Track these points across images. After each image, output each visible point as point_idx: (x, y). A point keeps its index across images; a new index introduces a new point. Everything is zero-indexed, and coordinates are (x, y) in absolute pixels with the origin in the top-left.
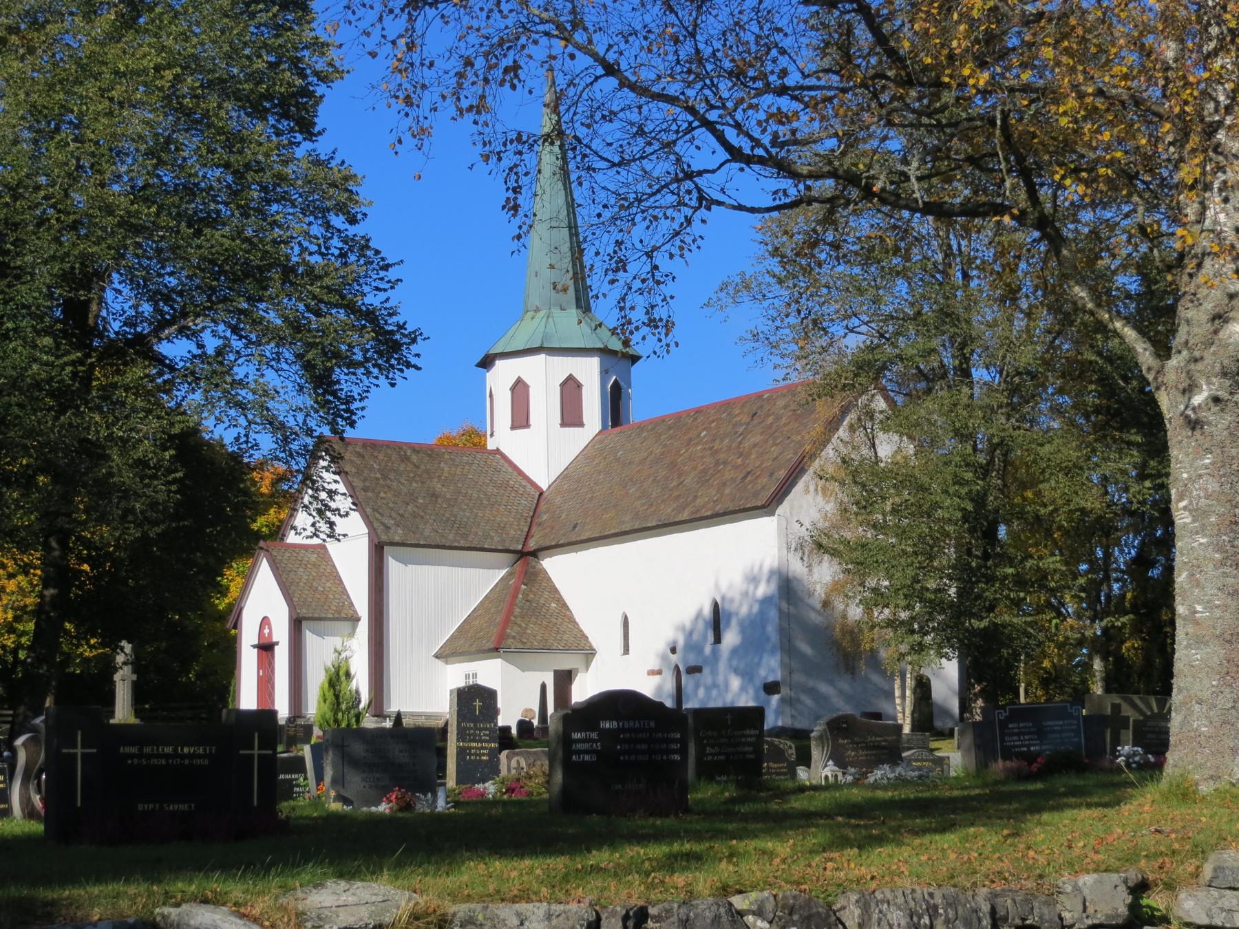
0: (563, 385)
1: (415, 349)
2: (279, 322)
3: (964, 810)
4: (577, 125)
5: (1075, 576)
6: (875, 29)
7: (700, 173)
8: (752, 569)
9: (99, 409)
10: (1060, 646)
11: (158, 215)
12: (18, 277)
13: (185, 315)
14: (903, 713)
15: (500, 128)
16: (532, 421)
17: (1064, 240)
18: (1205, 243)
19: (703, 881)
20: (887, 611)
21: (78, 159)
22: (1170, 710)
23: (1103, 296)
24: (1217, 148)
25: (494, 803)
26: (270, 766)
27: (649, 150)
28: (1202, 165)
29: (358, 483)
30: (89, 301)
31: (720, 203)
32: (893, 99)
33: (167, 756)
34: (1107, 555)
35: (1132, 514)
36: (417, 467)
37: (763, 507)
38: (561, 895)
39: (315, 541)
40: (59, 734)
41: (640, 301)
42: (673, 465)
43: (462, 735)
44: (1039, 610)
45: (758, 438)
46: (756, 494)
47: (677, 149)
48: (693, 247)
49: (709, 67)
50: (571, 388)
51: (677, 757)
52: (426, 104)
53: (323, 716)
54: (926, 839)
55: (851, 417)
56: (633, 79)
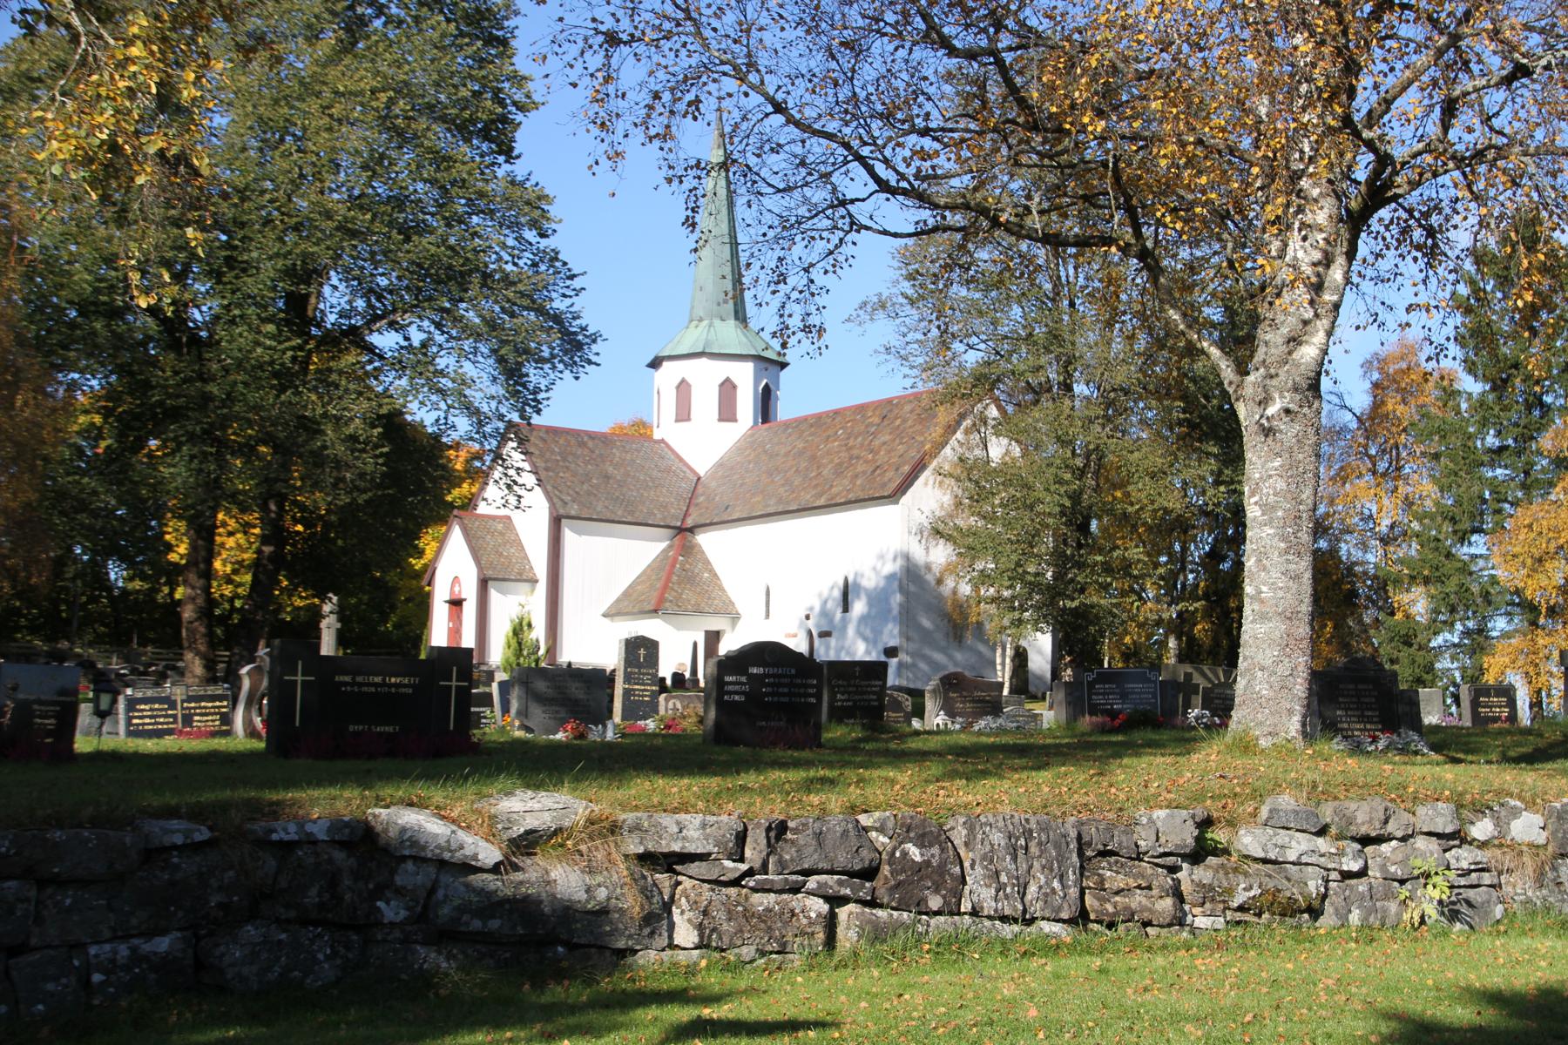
0: (722, 385)
1: (594, 348)
2: (477, 320)
3: (1056, 754)
4: (749, 154)
5: (1156, 565)
6: (1009, 82)
7: (852, 201)
9: (315, 389)
10: (1141, 625)
11: (373, 220)
12: (244, 270)
13: (394, 311)
14: (1003, 673)
15: (682, 156)
17: (1162, 270)
18: (1286, 275)
19: (835, 802)
20: (992, 590)
21: (301, 168)
22: (1235, 680)
23: (1193, 320)
24: (1299, 193)
25: (654, 735)
26: (465, 699)
27: (809, 179)
28: (1288, 205)
29: (541, 464)
30: (308, 296)
31: (867, 228)
32: (1020, 142)
33: (376, 685)
34: (1184, 549)
35: (1207, 514)
37: (889, 497)
38: (714, 809)
39: (503, 512)
40: (282, 663)
41: (797, 310)
42: (813, 458)
43: (628, 678)
44: (1124, 594)
45: (887, 438)
46: (884, 485)
47: (833, 179)
48: (845, 265)
49: (864, 109)
51: (813, 700)
52: (620, 132)
53: (507, 661)
54: (1024, 775)
55: (968, 422)
56: (798, 116)
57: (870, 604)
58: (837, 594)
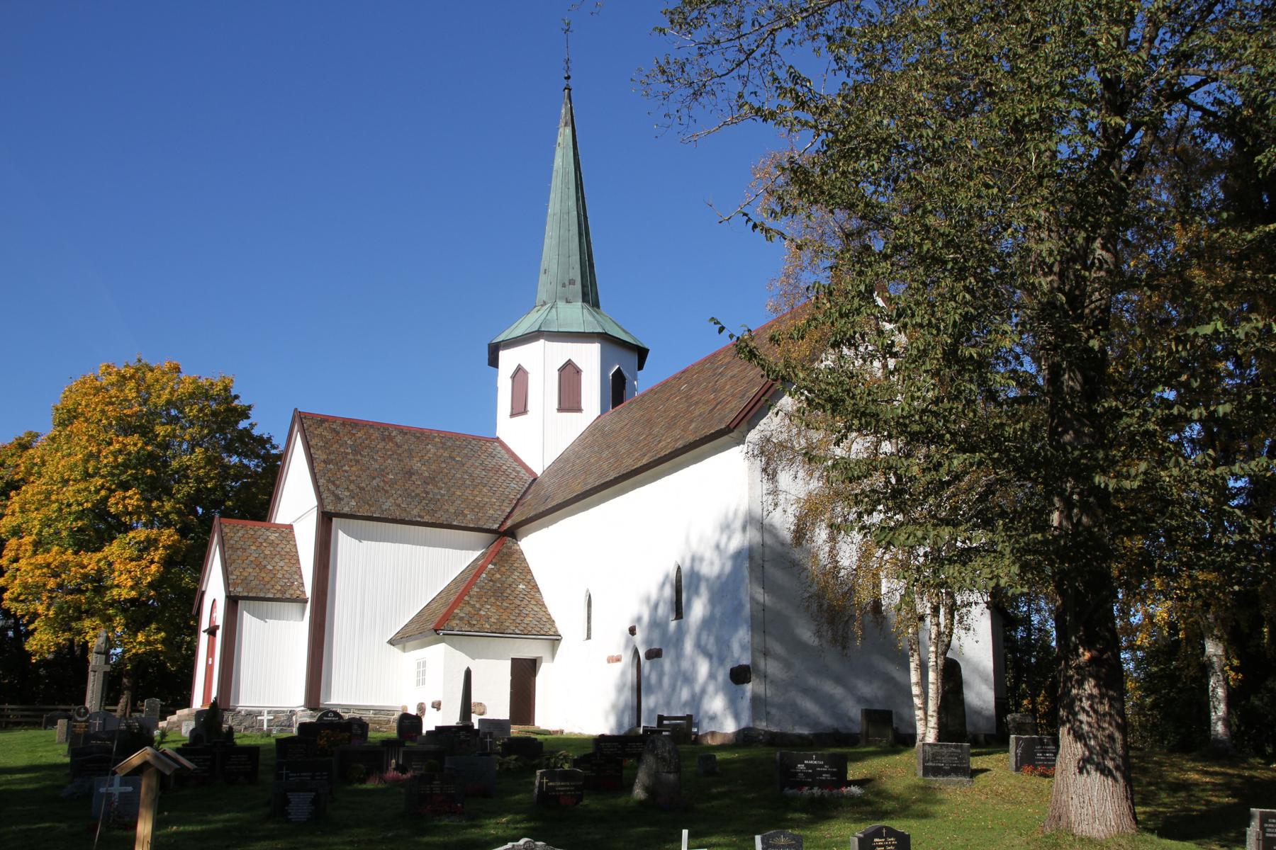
0: (561, 370)
8: (726, 517)
16: (529, 408)
36: (399, 447)
50: (569, 374)
57: (713, 601)
58: (669, 592)
